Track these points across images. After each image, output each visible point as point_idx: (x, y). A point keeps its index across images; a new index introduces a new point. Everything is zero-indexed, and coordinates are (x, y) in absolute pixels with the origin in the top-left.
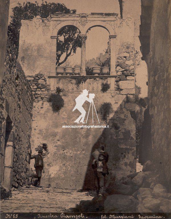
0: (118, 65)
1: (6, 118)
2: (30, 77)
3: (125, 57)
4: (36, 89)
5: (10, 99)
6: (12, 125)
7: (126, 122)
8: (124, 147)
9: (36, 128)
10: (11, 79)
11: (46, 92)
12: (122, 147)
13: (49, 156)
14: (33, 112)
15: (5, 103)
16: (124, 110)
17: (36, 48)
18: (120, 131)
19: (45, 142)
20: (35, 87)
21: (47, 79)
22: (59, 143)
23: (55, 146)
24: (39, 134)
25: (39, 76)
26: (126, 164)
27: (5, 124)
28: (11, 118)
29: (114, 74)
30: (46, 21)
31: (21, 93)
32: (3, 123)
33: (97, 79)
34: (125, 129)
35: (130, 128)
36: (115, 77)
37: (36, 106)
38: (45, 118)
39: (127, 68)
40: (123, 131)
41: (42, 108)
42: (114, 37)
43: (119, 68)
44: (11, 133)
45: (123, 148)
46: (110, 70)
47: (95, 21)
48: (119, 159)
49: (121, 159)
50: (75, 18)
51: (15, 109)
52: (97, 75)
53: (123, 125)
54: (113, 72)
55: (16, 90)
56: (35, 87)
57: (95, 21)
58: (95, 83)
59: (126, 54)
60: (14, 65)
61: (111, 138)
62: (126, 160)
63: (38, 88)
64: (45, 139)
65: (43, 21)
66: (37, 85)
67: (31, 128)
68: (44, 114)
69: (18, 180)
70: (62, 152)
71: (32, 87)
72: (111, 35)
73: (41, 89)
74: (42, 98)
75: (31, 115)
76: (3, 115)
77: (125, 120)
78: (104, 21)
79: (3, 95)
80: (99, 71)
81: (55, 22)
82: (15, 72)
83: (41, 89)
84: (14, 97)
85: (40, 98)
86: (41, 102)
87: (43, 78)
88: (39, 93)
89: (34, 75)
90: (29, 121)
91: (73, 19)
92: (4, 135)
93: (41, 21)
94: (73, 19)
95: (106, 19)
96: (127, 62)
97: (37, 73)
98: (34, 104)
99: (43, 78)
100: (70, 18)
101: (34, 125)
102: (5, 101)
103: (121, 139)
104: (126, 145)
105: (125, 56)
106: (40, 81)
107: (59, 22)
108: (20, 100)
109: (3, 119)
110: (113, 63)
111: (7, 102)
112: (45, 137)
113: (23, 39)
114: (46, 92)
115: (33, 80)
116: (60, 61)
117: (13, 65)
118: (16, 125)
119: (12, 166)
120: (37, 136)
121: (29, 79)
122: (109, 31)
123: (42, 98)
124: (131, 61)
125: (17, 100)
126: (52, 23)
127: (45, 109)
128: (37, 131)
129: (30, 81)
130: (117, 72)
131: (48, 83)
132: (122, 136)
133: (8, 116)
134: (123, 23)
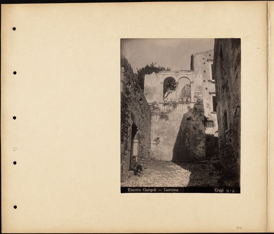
0: (195, 97)
1: (131, 125)
2: (150, 103)
3: (198, 93)
4: (153, 109)
5: (135, 113)
6: (137, 129)
7: (200, 126)
8: (199, 138)
9: (154, 129)
10: (136, 99)
11: (158, 111)
12: (198, 139)
13: (160, 143)
14: (152, 121)
15: (131, 114)
16: (199, 120)
17: (153, 89)
18: (197, 130)
19: (158, 137)
20: (153, 109)
21: (159, 104)
22: (165, 137)
23: (164, 139)
24: (155, 132)
25: (155, 103)
26: (200, 148)
27: (131, 129)
28: (136, 125)
29: (193, 101)
30: (158, 75)
31: (143, 109)
32: (129, 129)
33: (185, 104)
34: (199, 130)
35: (202, 129)
36: (194, 103)
37: (153, 118)
38: (158, 124)
39: (200, 98)
40: (199, 130)
41: (156, 119)
42: (193, 82)
43: (195, 98)
44: (137, 134)
45: (198, 139)
46: (191, 100)
47: (183, 74)
48: (197, 145)
49: (198, 145)
50: (173, 73)
51: (139, 119)
52: (185, 102)
53: (198, 127)
54: (193, 101)
55: (140, 107)
56: (153, 109)
57: (183, 74)
58: (184, 106)
59: (199, 91)
60: (138, 91)
61: (192, 134)
62: (200, 145)
63: (154, 109)
64: (158, 135)
65: (156, 75)
66: (154, 107)
67: (150, 130)
68: (157, 122)
69: (143, 161)
70: (167, 141)
71: (151, 108)
72: (191, 81)
73: (155, 109)
74: (156, 114)
75: (151, 123)
76: (129, 123)
77: (199, 125)
78: (187, 75)
79: (128, 108)
80: (186, 101)
81: (162, 75)
82: (139, 95)
83: (155, 109)
84: (139, 112)
85: (155, 114)
86: (156, 116)
87: (156, 104)
88: (155, 111)
89: (152, 102)
90: (150, 126)
91: (171, 73)
92: (131, 137)
93: (155, 75)
94: (171, 73)
95: (188, 74)
96: (199, 95)
97: (153, 101)
98: (152, 117)
99: (156, 104)
100: (170, 73)
101: (152, 128)
102: (130, 112)
103: (197, 134)
104: (200, 137)
105: (198, 92)
106: (155, 106)
107: (164, 75)
108: (143, 113)
109: (130, 125)
110: (192, 96)
111: (132, 114)
112: (158, 134)
113: (146, 84)
114: (158, 111)
115: (151, 105)
116: (165, 96)
117: (137, 91)
118: (141, 129)
119: (138, 155)
120: (154, 133)
121: (149, 104)
122: (189, 79)
123: (156, 114)
124: (201, 95)
125: (141, 113)
126: (160, 75)
127: (158, 120)
128: (154, 131)
129: (150, 105)
130: (195, 100)
131: (159, 106)
132: (197, 133)
133: (134, 123)
134: (197, 75)
